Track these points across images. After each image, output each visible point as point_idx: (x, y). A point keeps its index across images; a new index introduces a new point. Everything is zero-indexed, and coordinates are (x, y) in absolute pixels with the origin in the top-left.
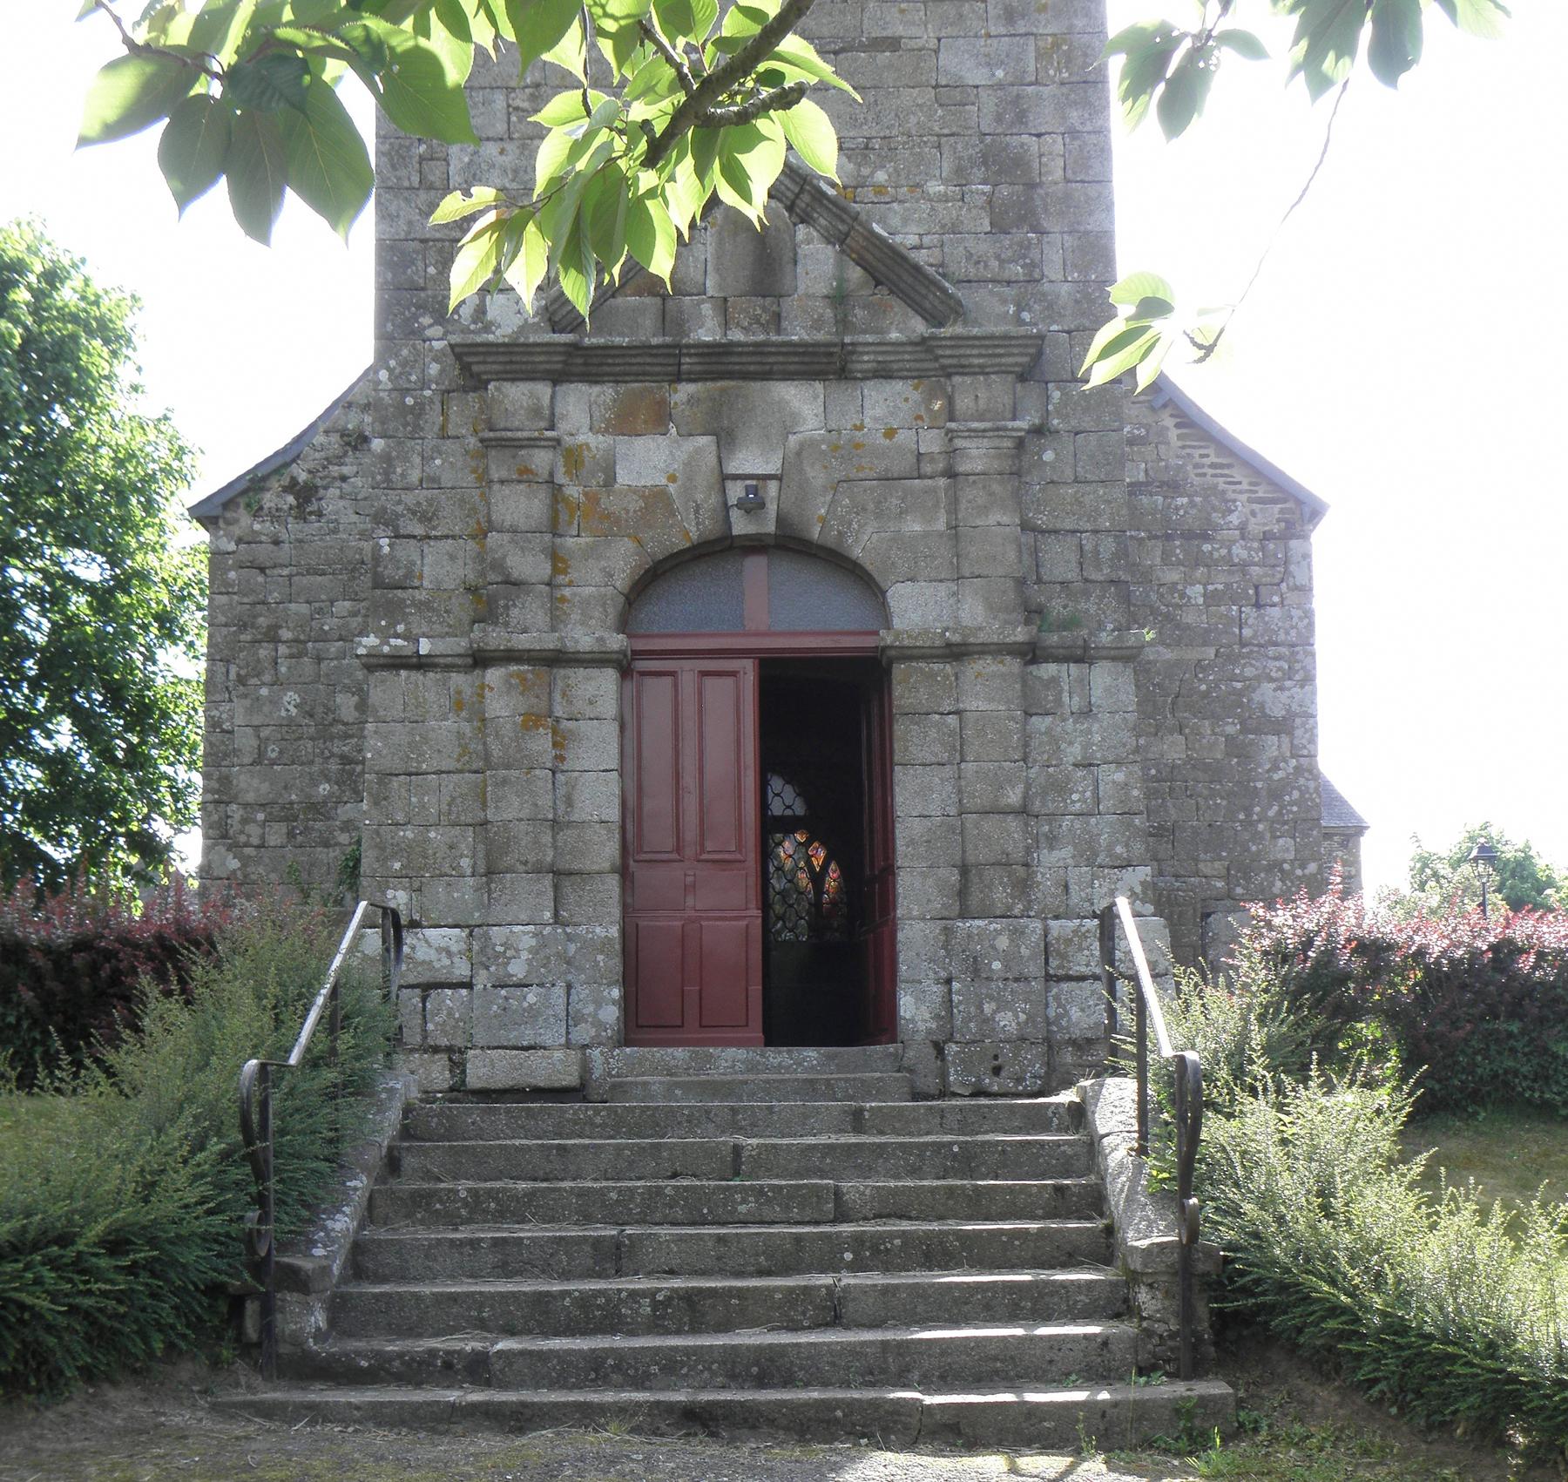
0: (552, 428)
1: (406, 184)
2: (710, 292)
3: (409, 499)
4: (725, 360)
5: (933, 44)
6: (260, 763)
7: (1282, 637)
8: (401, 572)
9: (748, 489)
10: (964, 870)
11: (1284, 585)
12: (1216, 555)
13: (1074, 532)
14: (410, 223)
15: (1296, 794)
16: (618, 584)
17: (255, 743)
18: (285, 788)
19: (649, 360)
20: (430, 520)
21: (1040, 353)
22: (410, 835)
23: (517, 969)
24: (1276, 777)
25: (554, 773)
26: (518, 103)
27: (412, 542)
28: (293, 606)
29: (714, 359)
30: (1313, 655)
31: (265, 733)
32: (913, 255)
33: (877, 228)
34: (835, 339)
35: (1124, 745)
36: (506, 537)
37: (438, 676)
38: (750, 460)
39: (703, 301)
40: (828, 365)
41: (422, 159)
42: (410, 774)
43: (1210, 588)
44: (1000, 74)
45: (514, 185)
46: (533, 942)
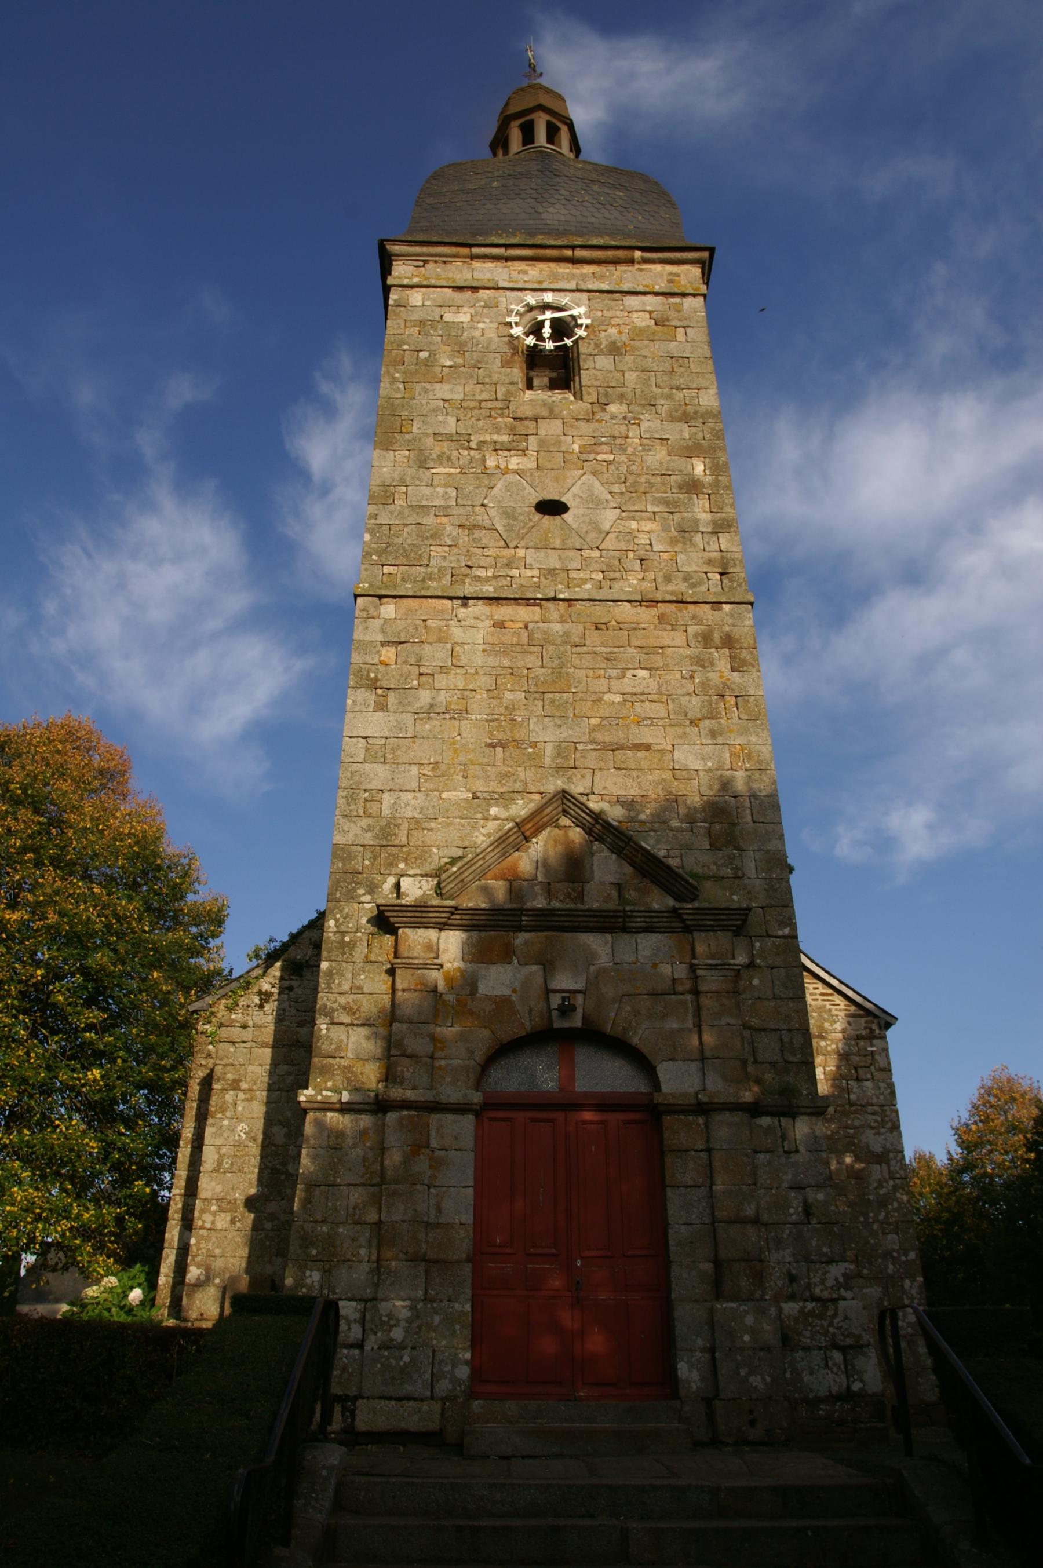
0: (437, 958)
1: (355, 814)
2: (540, 879)
3: (342, 1000)
4: (549, 918)
5: (670, 747)
6: (218, 1171)
7: (875, 1101)
8: (333, 1047)
9: (564, 999)
10: (717, 1263)
11: (872, 1068)
12: (829, 1048)
13: (776, 1030)
14: (356, 835)
15: (895, 1204)
16: (477, 1059)
17: (217, 1157)
18: (233, 1189)
19: (501, 918)
20: (354, 1013)
21: (744, 921)
22: (325, 1229)
23: (397, 1334)
24: (881, 1192)
25: (429, 1188)
26: (425, 772)
27: (342, 1027)
28: (250, 1068)
29: (543, 918)
30: (897, 1112)
31: (224, 1150)
32: (664, 860)
33: (644, 844)
34: (621, 908)
35: (821, 1174)
36: (405, 1026)
37: (353, 1117)
38: (564, 981)
39: (536, 885)
40: (612, 922)
41: (366, 800)
42: (329, 1186)
43: (828, 1069)
44: (709, 764)
45: (420, 816)
46: (409, 1314)
